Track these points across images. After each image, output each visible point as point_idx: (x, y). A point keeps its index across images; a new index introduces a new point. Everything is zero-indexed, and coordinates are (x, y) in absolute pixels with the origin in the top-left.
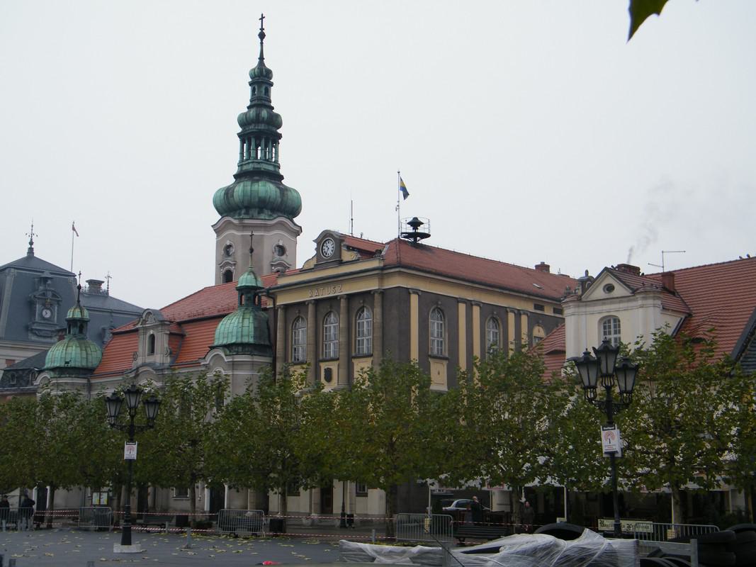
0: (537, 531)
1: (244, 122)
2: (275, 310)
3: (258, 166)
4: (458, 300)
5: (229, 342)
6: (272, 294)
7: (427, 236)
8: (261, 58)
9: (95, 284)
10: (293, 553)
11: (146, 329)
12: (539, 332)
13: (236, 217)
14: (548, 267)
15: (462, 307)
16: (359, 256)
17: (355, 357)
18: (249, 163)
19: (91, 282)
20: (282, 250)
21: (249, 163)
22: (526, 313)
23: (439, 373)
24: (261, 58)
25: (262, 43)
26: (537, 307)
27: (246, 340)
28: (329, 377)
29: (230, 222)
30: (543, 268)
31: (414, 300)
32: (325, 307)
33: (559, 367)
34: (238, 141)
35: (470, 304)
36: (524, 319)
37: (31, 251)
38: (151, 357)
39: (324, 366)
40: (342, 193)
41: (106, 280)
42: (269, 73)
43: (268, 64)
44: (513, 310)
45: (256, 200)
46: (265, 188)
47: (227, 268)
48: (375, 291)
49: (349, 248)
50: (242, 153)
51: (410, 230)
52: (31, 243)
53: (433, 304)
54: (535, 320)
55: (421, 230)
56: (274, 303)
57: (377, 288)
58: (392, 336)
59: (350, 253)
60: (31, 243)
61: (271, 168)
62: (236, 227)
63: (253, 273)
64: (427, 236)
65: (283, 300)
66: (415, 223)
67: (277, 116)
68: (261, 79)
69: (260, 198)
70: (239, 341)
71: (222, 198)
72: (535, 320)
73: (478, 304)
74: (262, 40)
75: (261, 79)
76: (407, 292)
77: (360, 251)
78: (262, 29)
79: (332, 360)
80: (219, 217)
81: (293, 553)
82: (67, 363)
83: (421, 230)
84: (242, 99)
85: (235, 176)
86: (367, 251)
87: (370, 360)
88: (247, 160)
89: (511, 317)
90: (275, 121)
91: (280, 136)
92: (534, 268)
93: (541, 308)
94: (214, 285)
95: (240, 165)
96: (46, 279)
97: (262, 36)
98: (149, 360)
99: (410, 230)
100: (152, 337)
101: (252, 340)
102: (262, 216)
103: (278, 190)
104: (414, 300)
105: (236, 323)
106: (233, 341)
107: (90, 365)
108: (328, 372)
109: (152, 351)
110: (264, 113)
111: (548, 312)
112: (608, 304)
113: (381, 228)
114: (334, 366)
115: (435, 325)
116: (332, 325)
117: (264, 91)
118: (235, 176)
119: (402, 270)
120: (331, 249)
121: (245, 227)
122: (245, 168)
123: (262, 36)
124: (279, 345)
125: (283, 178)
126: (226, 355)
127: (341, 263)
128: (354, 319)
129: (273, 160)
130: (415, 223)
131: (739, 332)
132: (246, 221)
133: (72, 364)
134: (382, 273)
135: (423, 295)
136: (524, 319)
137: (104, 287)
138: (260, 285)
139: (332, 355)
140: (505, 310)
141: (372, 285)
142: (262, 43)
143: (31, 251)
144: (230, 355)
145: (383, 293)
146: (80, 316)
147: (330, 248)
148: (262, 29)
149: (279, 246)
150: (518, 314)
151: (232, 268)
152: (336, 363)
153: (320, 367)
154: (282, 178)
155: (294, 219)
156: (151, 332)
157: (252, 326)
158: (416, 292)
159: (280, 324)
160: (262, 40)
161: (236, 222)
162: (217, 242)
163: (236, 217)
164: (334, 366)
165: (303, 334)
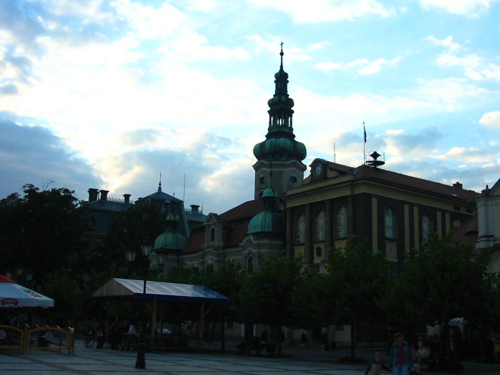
0: (122, 293)
1: (271, 103)
2: (285, 210)
4: (404, 203)
5: (256, 231)
6: (283, 200)
7: (383, 163)
8: (282, 67)
9: (195, 208)
10: (452, 348)
12: (457, 224)
13: (267, 160)
14: (461, 185)
15: (406, 207)
16: (338, 174)
17: (336, 240)
18: (274, 128)
19: (193, 206)
21: (274, 128)
22: (448, 211)
23: (391, 250)
24: (282, 67)
25: (282, 58)
26: (455, 208)
27: (267, 230)
28: (319, 254)
29: (263, 163)
30: (458, 186)
31: (374, 201)
32: (316, 208)
34: (268, 116)
35: (411, 205)
36: (447, 216)
37: (160, 188)
39: (316, 246)
40: (326, 136)
42: (286, 75)
43: (285, 70)
44: (440, 210)
45: (279, 148)
46: (282, 141)
48: (348, 196)
49: (331, 169)
50: (270, 122)
51: (372, 159)
53: (385, 204)
54: (454, 216)
55: (379, 159)
56: (285, 207)
57: (349, 194)
58: (360, 225)
59: (332, 172)
60: (160, 184)
61: (287, 131)
62: (267, 166)
63: (272, 188)
64: (383, 163)
65: (290, 204)
66: (375, 155)
67: (292, 100)
68: (282, 79)
70: (263, 230)
71: (258, 149)
72: (454, 216)
73: (417, 205)
74: (282, 56)
75: (282, 79)
76: (369, 196)
77: (339, 171)
78: (282, 50)
79: (322, 242)
80: (257, 160)
81: (452, 348)
82: (166, 246)
83: (379, 159)
84: (270, 91)
85: (266, 136)
86: (342, 170)
87: (345, 241)
88: (273, 126)
89: (439, 214)
90: (291, 103)
91: (293, 112)
92: (452, 186)
93: (459, 209)
94: (253, 199)
95: (269, 129)
97: (282, 54)
98: (212, 244)
99: (372, 159)
100: (213, 230)
101: (270, 230)
102: (282, 159)
103: (291, 143)
104: (374, 201)
105: (261, 219)
106: (259, 230)
108: (319, 250)
109: (213, 239)
110: (283, 98)
111: (463, 211)
113: (353, 158)
114: (322, 246)
115: (389, 220)
117: (283, 86)
118: (266, 136)
119: (367, 181)
120: (320, 170)
121: (271, 166)
122: (272, 131)
123: (282, 54)
124: (288, 233)
125: (295, 137)
126: (254, 240)
129: (289, 126)
130: (375, 155)
132: (273, 162)
133: (168, 247)
134: (353, 184)
135: (380, 199)
136: (447, 216)
137: (200, 209)
138: (276, 195)
139: (321, 238)
140: (435, 210)
141: (347, 192)
142: (282, 58)
143: (160, 188)
144: (257, 239)
145: (354, 197)
146: (173, 219)
147: (319, 169)
148: (282, 50)
149: (292, 177)
150: (444, 212)
152: (324, 244)
153: (313, 247)
154: (294, 136)
155: (302, 161)
156: (212, 227)
157: (270, 221)
158: (376, 196)
159: (288, 220)
160: (282, 56)
161: (267, 163)
162: (256, 176)
163: (267, 160)
164: (322, 246)
165: (302, 226)
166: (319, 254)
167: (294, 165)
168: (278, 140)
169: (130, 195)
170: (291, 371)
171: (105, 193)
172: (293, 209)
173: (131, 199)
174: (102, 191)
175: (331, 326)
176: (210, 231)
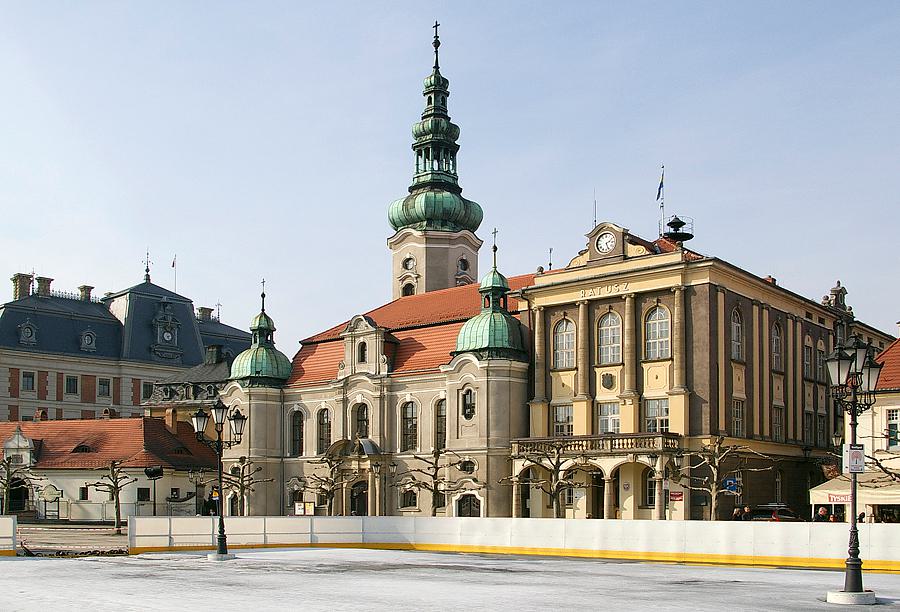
3: (439, 178)
4: (753, 302)
7: (690, 237)
9: (206, 311)
11: (355, 337)
19: (202, 310)
20: (465, 264)
25: (437, 52)
33: (821, 392)
35: (762, 307)
38: (362, 365)
41: (216, 309)
47: (407, 282)
52: (147, 270)
60: (147, 270)
61: (451, 180)
64: (690, 237)
66: (677, 224)
68: (439, 89)
69: (444, 209)
74: (436, 48)
75: (439, 89)
83: (681, 230)
90: (453, 131)
94: (12, 300)
96: (165, 304)
97: (437, 44)
100: (363, 345)
101: (506, 345)
107: (281, 377)
109: (362, 359)
112: (584, 383)
114: (615, 372)
116: (657, 322)
123: (437, 44)
127: (626, 258)
128: (596, 326)
130: (677, 224)
131: (816, 406)
132: (430, 233)
137: (214, 314)
141: (674, 281)
147: (607, 243)
149: (462, 260)
151: (414, 282)
156: (362, 339)
160: (436, 48)
164: (615, 372)
166: (609, 382)
167: (464, 239)
168: (439, 196)
169: (840, 293)
170: (395, 567)
171: (45, 282)
172: (547, 311)
173: (93, 294)
174: (40, 280)
175: (297, 504)
176: (356, 348)
